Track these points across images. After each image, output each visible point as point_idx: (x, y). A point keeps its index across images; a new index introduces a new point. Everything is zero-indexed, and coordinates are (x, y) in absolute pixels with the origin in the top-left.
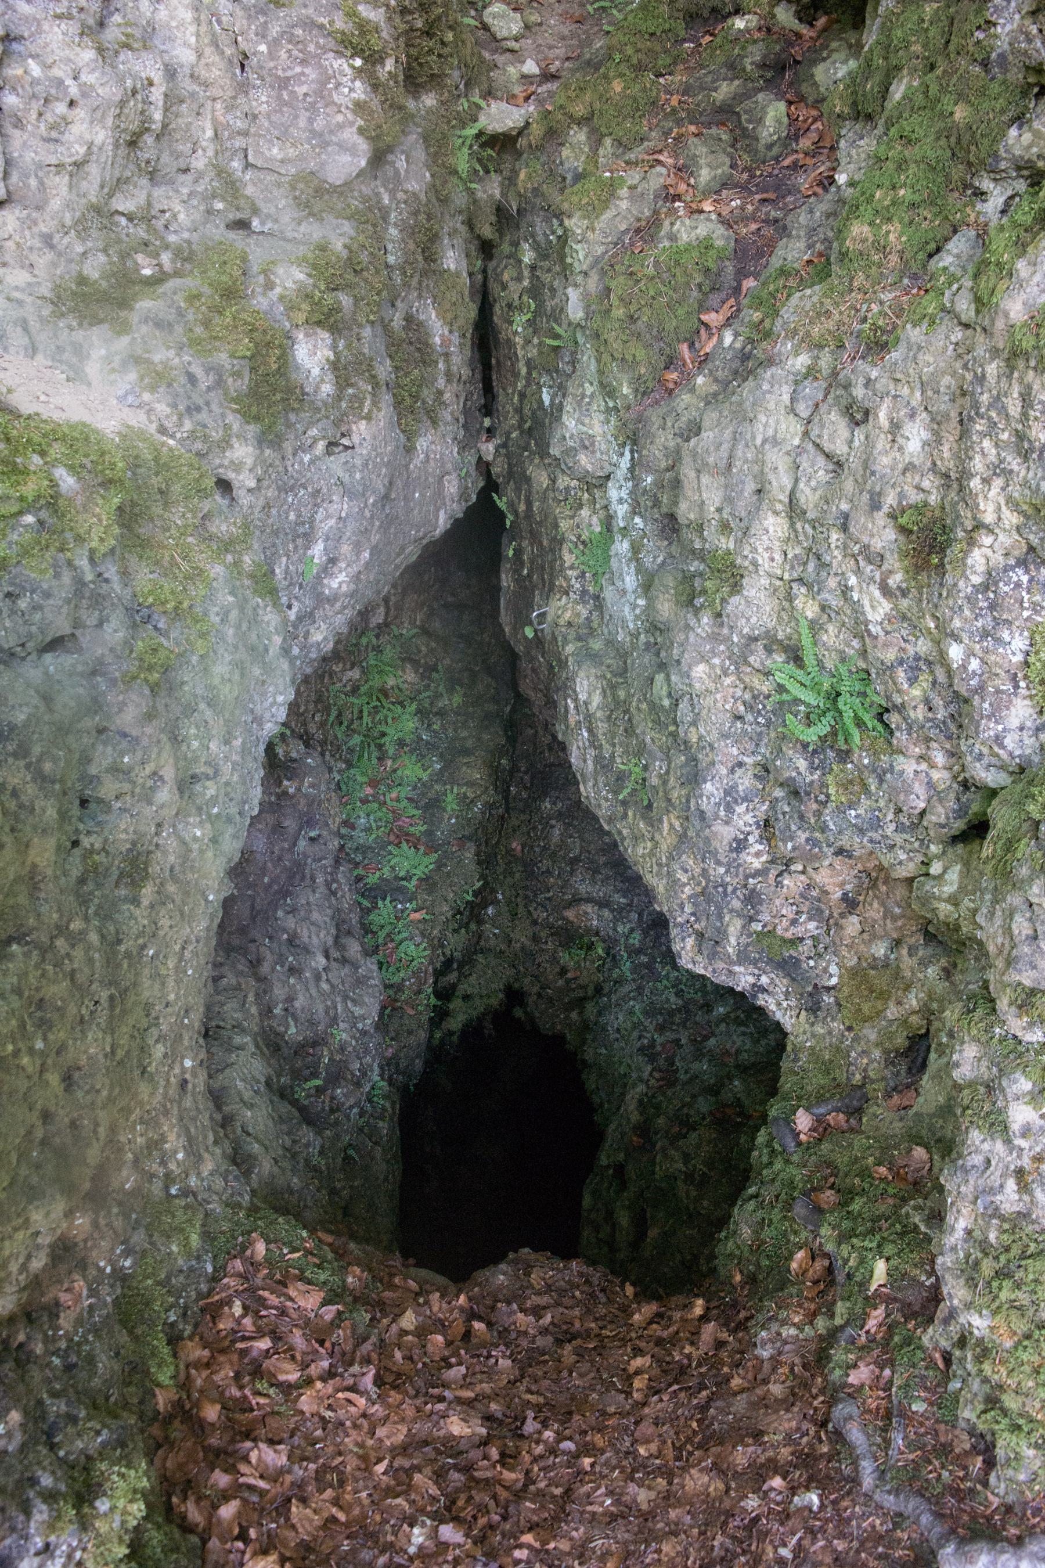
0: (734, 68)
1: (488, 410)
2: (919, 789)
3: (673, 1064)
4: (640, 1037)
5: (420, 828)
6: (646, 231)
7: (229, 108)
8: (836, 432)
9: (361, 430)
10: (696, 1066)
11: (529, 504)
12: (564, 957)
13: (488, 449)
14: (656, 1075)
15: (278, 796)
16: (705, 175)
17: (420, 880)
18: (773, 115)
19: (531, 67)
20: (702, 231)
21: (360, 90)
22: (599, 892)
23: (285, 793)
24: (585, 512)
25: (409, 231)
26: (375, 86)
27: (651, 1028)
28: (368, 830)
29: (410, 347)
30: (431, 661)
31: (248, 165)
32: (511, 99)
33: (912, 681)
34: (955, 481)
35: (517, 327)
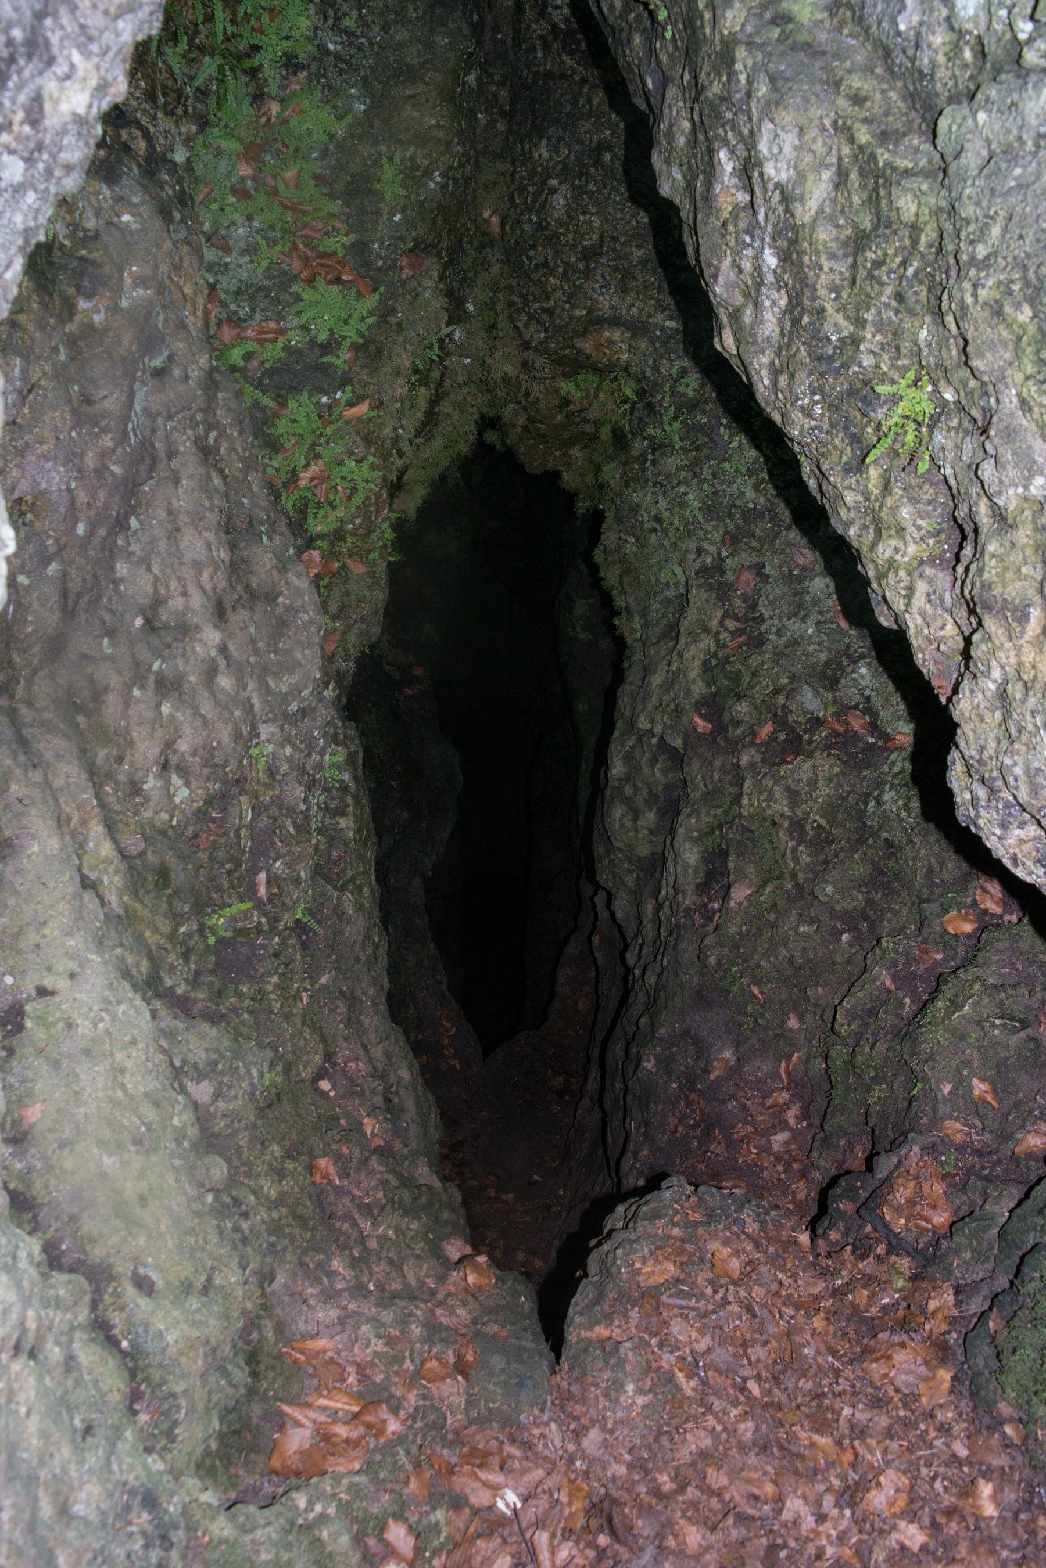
3: (754, 606)
4: (700, 551)
5: (340, 242)
10: (794, 626)
12: (565, 386)
14: (730, 624)
15: (72, 342)
17: (355, 347)
22: (632, 309)
23: (89, 328)
27: (717, 536)
28: (251, 250)
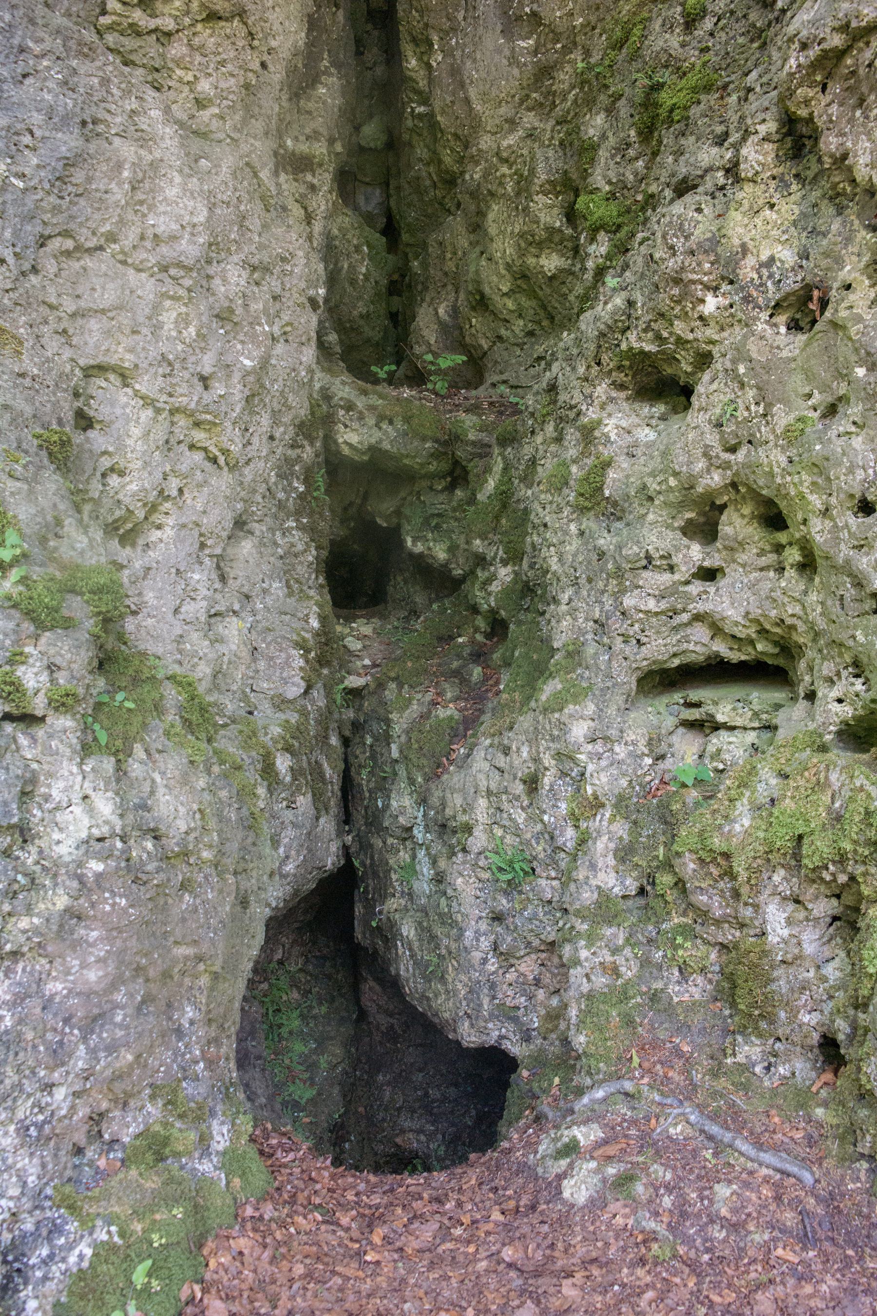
0: (459, 656)
1: (347, 822)
2: (548, 890)
6: (424, 717)
7: (248, 668)
8: (501, 761)
9: (300, 799)
11: (372, 858)
13: (349, 839)
16: (449, 695)
18: (477, 672)
19: (367, 662)
20: (449, 713)
21: (302, 663)
24: (401, 853)
25: (318, 722)
26: (307, 661)
29: (317, 771)
30: (308, 987)
31: (253, 691)
32: (359, 675)
33: (538, 843)
34: (536, 760)
35: (363, 777)
